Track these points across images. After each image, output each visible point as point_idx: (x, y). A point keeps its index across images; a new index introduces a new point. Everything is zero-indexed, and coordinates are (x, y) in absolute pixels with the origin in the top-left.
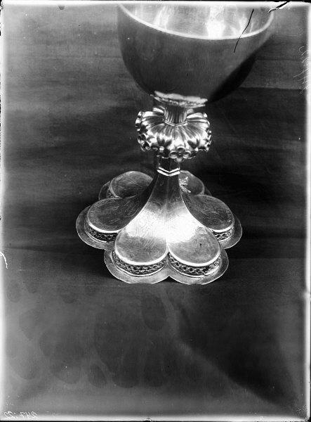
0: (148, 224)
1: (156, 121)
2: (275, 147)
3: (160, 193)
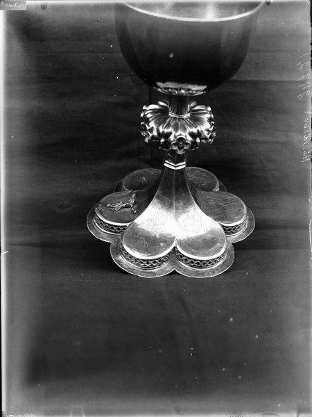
0: (156, 219)
1: (161, 115)
2: (271, 139)
3: (175, 190)
